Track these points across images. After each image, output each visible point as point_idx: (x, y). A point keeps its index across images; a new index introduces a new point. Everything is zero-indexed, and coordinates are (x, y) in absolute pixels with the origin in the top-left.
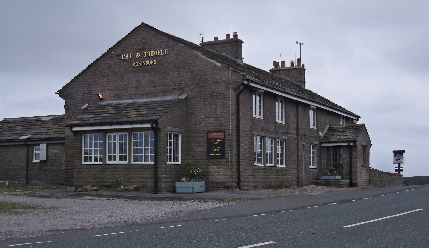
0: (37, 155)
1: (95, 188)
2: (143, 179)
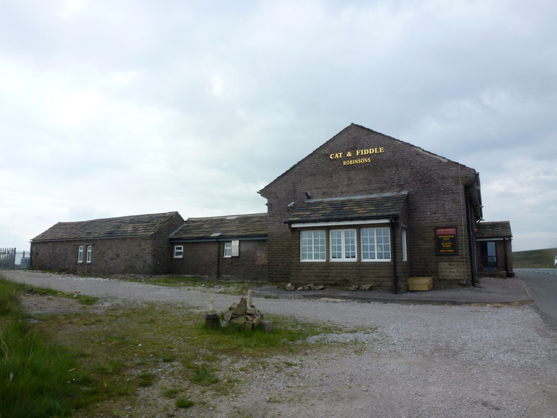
0: (227, 250)
1: (321, 287)
2: (378, 277)
